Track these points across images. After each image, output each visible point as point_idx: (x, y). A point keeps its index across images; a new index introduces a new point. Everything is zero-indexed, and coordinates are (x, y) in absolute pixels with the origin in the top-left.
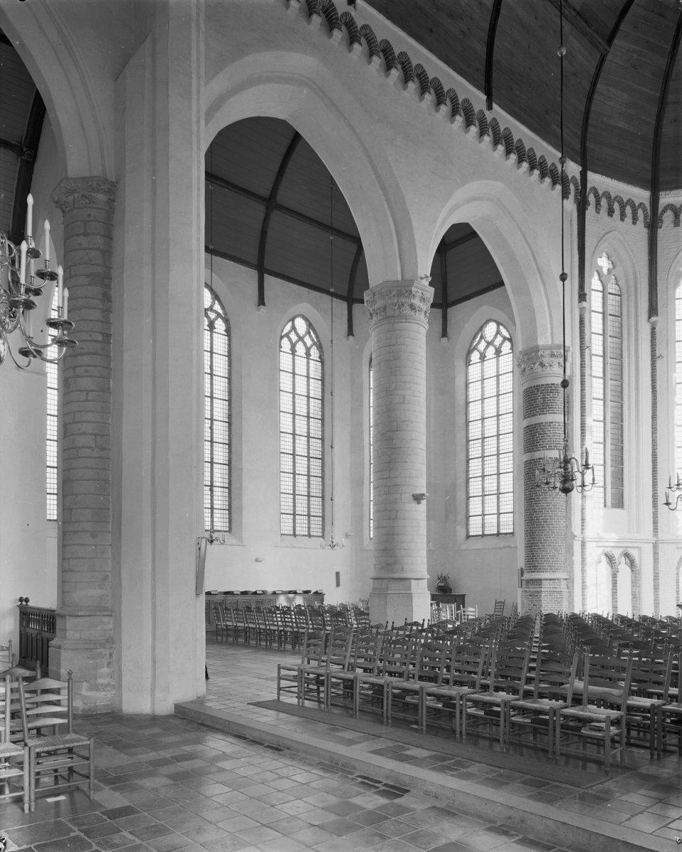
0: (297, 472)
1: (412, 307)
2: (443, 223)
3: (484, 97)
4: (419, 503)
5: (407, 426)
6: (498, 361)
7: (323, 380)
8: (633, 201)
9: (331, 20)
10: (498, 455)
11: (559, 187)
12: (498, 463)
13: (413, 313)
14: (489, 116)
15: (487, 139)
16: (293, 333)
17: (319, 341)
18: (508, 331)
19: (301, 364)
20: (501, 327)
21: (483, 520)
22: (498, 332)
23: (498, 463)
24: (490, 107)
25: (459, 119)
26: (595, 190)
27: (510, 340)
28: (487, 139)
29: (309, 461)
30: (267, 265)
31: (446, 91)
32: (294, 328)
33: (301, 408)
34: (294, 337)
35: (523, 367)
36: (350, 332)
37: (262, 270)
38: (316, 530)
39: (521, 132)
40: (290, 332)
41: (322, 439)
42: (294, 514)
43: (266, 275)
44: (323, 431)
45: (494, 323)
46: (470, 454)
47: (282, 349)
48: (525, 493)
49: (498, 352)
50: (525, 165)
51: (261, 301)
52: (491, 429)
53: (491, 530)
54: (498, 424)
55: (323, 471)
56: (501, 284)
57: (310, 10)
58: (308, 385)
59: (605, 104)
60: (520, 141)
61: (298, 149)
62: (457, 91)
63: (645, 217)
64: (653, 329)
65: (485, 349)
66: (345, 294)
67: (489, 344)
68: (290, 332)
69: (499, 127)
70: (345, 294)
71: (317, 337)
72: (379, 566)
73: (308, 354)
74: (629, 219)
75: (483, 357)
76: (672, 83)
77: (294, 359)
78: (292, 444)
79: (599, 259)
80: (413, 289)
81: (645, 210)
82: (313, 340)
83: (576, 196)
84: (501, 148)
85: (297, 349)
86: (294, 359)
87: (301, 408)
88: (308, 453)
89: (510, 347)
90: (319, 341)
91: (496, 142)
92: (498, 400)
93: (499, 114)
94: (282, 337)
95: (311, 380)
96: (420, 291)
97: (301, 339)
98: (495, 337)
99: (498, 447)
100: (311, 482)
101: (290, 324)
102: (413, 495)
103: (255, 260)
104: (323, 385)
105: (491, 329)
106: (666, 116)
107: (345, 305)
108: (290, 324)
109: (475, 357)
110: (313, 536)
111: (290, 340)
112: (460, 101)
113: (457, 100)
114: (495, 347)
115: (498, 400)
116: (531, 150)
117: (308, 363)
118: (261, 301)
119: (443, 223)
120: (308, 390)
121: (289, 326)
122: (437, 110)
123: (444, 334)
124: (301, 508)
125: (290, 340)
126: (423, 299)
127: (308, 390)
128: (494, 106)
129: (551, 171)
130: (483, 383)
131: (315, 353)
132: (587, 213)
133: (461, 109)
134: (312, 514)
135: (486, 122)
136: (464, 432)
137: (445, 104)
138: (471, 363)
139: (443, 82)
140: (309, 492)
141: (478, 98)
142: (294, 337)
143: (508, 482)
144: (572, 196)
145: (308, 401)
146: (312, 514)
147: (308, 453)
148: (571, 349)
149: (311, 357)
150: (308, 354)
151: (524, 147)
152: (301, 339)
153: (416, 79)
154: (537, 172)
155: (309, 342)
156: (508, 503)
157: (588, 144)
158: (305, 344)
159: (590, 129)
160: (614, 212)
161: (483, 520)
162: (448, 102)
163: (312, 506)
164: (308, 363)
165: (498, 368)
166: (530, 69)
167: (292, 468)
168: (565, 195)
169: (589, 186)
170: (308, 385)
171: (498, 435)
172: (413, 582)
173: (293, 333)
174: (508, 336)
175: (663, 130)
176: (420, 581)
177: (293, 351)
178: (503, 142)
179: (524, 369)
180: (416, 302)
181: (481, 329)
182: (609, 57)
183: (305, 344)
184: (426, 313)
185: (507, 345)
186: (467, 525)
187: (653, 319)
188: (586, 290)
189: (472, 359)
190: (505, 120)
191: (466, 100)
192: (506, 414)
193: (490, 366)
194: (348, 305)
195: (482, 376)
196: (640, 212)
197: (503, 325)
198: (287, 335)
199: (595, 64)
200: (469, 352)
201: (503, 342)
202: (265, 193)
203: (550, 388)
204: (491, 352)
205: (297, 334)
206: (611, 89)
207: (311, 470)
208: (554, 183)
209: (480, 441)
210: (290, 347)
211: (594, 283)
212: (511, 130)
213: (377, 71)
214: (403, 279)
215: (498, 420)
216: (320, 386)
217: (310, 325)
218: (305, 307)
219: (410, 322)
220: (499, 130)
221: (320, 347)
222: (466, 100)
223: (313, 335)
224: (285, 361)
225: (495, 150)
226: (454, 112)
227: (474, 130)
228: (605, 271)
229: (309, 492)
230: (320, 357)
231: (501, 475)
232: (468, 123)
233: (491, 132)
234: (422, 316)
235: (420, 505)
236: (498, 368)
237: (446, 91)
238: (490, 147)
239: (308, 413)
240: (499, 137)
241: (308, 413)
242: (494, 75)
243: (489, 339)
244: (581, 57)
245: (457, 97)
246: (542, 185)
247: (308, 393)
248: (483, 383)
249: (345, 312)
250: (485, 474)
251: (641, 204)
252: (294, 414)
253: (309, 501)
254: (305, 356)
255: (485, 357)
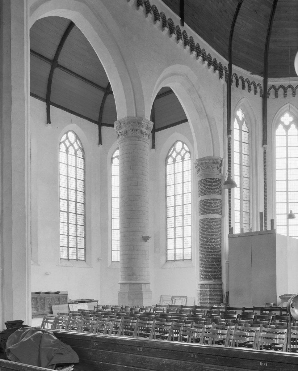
0: (70, 222)
1: (141, 132)
2: (158, 86)
3: (180, 19)
4: (146, 241)
5: (139, 198)
6: (183, 164)
7: (84, 170)
8: (255, 82)
9: (149, 9)
10: (183, 215)
11: (217, 72)
12: (183, 220)
13: (142, 135)
14: (182, 29)
15: (181, 42)
16: (67, 141)
17: (82, 146)
18: (188, 147)
19: (72, 159)
20: (184, 145)
21: (175, 251)
22: (183, 148)
23: (183, 220)
24: (182, 25)
25: (167, 29)
26: (236, 75)
27: (190, 152)
28: (181, 42)
29: (76, 216)
30: (52, 100)
31: (159, 13)
32: (67, 138)
33: (72, 185)
34: (68, 144)
35: (198, 168)
36: (100, 142)
37: (49, 102)
38: (81, 257)
39: (198, 40)
40: (65, 140)
41: (84, 204)
42: (68, 247)
43: (51, 106)
44: (85, 199)
45: (181, 142)
46: (168, 214)
47: (60, 150)
48: (200, 237)
49: (183, 159)
50: (201, 58)
51: (49, 121)
52: (179, 202)
53: (179, 257)
54: (183, 198)
55: (85, 222)
56: (186, 120)
57: (139, 4)
58: (76, 172)
59: (241, 29)
60: (198, 44)
61: (71, 33)
62: (165, 14)
63: (261, 91)
64: (265, 152)
65: (176, 157)
66: (97, 120)
67: (179, 153)
68: (65, 140)
69: (187, 36)
70: (97, 120)
71: (81, 144)
72: (124, 277)
73: (76, 154)
74: (252, 92)
75: (174, 161)
76: (274, 21)
77: (67, 156)
78: (66, 206)
79: (243, 117)
80: (142, 122)
81: (260, 87)
82: (78, 146)
83: (226, 77)
84: (188, 47)
85: (69, 150)
86: (67, 156)
87: (72, 185)
88: (76, 211)
89: (189, 156)
90: (82, 146)
91: (185, 44)
92: (183, 185)
93: (187, 28)
94: (60, 143)
95: (78, 169)
96: (146, 124)
97: (72, 144)
98: (181, 150)
99: (183, 211)
100: (78, 228)
101: (65, 135)
102: (143, 237)
103: (44, 96)
104: (85, 172)
105: (179, 146)
106: (271, 38)
107: (97, 126)
108: (65, 135)
109: (170, 160)
110: (79, 260)
111: (65, 145)
112: (167, 20)
113: (166, 19)
114: (181, 155)
115: (183, 185)
116: (204, 50)
117: (76, 159)
118: (49, 121)
119: (158, 86)
120: (76, 174)
121: (64, 137)
122: (155, 23)
123: (100, 142)
124: (72, 244)
125: (65, 145)
126: (147, 128)
127: (76, 174)
128: (185, 24)
129: (214, 62)
130: (175, 175)
131: (80, 153)
132: (232, 86)
133: (167, 24)
134: (78, 247)
135: (181, 32)
136: (165, 203)
137: (159, 20)
138: (168, 164)
139: (174, 22)
140: (77, 234)
141: (176, 19)
142: (67, 143)
143: (188, 231)
144: (224, 77)
145: (76, 182)
146: (78, 247)
147: (76, 211)
148: (224, 160)
149: (77, 156)
150: (76, 154)
151: (200, 48)
152: (72, 144)
153: (143, 5)
154: (206, 62)
155: (76, 146)
156: (188, 242)
157: (233, 50)
158: (74, 148)
159: (233, 41)
160: (239, 84)
161: (175, 251)
162: (161, 19)
163: (78, 242)
164: (76, 159)
165: (183, 168)
166: (203, 6)
167: (67, 220)
168: (221, 77)
169: (233, 73)
170: (76, 172)
171: (183, 205)
172: (143, 286)
173: (67, 141)
174: (188, 150)
175: (269, 46)
176: (146, 285)
177: (67, 151)
178: (189, 44)
179: (199, 169)
180: (144, 129)
181: (174, 145)
182: (243, 4)
183: (74, 148)
184: (149, 136)
185: (188, 155)
186: (166, 254)
187: (265, 146)
188: (231, 129)
189: (168, 161)
190: (191, 33)
191: (170, 19)
192: (187, 193)
193: (179, 166)
194: (99, 127)
195: (174, 172)
196: (258, 88)
197: (185, 144)
198: (64, 142)
199: (236, 7)
200: (167, 158)
201: (186, 153)
202: (51, 56)
203: (219, 181)
204: (179, 158)
205: (70, 142)
206: (244, 21)
207: (78, 221)
208: (215, 69)
209: (173, 207)
210: (65, 149)
211: (235, 125)
212: (187, 32)
213: (194, 57)
214: (136, 116)
215: (183, 196)
216: (83, 173)
217: (77, 137)
218: (74, 126)
219: (140, 141)
220: (187, 38)
221: (83, 150)
222: (170, 19)
223: (79, 143)
224: (62, 157)
225: (185, 48)
226: (164, 25)
227: (174, 36)
228: (241, 119)
229: (77, 234)
230: (83, 156)
231: (184, 227)
232: (171, 32)
233: (183, 39)
234: (147, 137)
235: (146, 243)
236: (183, 168)
237: (159, 13)
238: (182, 47)
239: (76, 188)
240: (187, 41)
241: (76, 188)
242: (185, 7)
243: (178, 151)
244: (229, 3)
245: (165, 17)
246: (191, 55)
247: (76, 176)
248: (175, 175)
249: (97, 131)
250: (176, 226)
251: (259, 84)
252: (68, 188)
253: (77, 239)
254: (74, 155)
255: (176, 161)
